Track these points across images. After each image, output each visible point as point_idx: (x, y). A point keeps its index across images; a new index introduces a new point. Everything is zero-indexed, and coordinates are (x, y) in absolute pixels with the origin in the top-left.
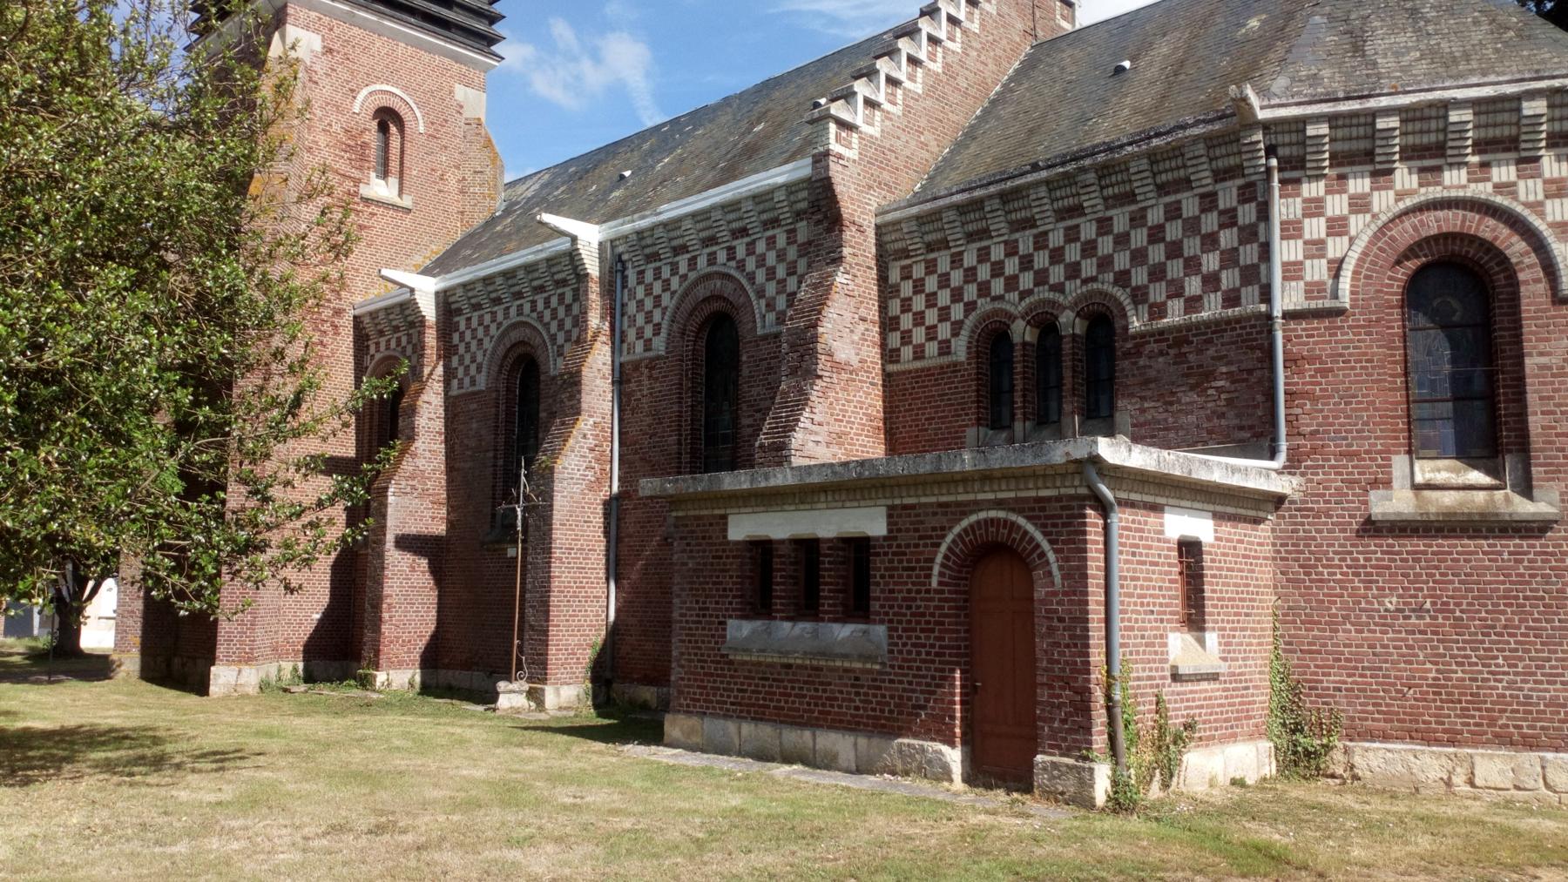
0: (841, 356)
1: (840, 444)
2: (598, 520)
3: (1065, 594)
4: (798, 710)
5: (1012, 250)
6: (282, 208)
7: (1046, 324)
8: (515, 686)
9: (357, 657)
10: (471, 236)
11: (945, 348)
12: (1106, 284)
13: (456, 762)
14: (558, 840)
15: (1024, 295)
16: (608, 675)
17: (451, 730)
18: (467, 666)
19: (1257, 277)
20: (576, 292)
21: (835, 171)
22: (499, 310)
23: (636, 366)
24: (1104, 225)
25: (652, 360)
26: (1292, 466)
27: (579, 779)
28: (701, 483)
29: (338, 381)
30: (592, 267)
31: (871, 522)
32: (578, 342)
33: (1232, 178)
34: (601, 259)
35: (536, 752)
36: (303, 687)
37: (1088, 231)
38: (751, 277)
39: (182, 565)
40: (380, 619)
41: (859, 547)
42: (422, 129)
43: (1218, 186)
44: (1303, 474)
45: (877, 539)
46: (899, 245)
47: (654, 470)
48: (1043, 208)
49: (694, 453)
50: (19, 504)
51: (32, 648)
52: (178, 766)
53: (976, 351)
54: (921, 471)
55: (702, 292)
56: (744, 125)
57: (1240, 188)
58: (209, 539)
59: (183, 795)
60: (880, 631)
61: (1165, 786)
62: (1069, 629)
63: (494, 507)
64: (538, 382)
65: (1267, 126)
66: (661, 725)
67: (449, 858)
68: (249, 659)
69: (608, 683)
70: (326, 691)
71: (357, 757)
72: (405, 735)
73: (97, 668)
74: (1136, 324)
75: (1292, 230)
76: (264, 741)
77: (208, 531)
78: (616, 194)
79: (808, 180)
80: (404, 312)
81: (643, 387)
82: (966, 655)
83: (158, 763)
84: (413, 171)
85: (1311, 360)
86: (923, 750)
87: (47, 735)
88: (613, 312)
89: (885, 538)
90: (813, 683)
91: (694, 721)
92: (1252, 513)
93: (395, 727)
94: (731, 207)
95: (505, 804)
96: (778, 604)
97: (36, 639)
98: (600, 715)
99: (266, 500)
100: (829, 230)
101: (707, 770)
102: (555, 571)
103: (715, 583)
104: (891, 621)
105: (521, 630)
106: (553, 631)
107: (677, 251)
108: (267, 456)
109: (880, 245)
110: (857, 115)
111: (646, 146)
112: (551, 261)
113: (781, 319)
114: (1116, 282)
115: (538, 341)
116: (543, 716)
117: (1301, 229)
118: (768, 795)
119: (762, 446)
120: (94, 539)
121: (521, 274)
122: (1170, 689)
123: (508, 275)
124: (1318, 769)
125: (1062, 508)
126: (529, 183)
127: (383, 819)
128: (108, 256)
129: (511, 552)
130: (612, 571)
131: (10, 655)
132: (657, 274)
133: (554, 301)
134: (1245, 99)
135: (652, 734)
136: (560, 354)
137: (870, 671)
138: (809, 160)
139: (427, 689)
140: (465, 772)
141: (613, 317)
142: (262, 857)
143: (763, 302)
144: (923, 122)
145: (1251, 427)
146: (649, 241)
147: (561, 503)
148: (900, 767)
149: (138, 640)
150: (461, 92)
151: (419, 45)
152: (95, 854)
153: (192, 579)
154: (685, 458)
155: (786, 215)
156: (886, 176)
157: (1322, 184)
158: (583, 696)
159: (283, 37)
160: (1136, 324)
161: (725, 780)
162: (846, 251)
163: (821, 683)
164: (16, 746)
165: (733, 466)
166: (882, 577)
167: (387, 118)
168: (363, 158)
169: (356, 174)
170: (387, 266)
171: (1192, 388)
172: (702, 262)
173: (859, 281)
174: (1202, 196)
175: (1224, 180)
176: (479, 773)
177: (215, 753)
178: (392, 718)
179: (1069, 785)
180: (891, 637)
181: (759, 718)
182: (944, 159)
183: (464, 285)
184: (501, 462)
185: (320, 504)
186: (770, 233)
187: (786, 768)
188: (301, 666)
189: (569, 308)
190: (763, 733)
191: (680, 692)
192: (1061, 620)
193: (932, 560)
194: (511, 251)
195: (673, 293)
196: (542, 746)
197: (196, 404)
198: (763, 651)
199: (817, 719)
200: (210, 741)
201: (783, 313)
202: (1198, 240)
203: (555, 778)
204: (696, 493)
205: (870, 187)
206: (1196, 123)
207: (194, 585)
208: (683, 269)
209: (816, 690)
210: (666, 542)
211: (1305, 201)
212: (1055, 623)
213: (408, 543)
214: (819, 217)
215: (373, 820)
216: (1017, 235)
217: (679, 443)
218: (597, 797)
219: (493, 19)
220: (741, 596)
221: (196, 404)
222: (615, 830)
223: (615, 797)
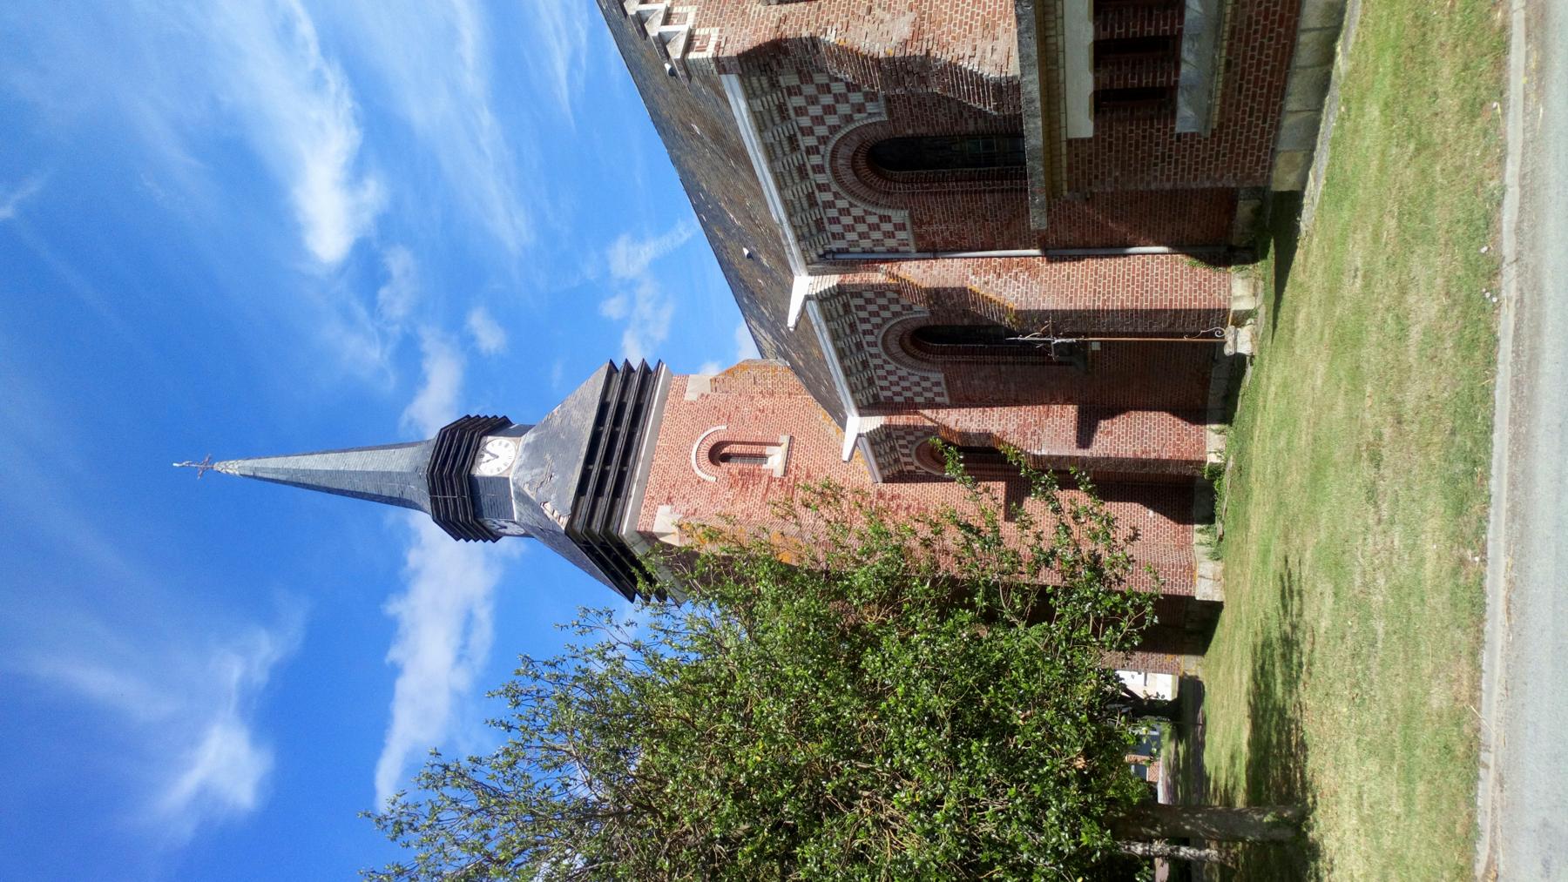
0: (906, 32)
1: (994, 25)
2: (1067, 267)
4: (1276, 50)
6: (804, 537)
8: (1229, 339)
9: (1191, 479)
10: (809, 387)
13: (1307, 390)
14: (1403, 291)
16: (1223, 250)
17: (1271, 396)
18: (1205, 382)
20: (853, 295)
21: (731, 50)
22: (873, 362)
23: (919, 237)
25: (913, 223)
27: (1336, 276)
28: (1036, 167)
29: (950, 497)
30: (831, 281)
32: (899, 292)
34: (824, 273)
35: (1302, 316)
36: (1218, 525)
38: (834, 129)
39: (1112, 620)
40: (1156, 460)
47: (1022, 213)
49: (1001, 177)
50: (1062, 741)
51: (1171, 738)
52: (1294, 627)
55: (849, 177)
56: (695, 143)
58: (1088, 600)
59: (1325, 624)
63: (1052, 363)
64: (936, 327)
66: (1282, 196)
67: (1411, 397)
68: (1190, 569)
69: (1231, 249)
70: (1224, 504)
71: (1295, 478)
72: (1274, 436)
73: (1191, 691)
76: (1272, 557)
77: (1082, 600)
78: (764, 261)
79: (741, 77)
80: (878, 442)
81: (939, 230)
83: (1289, 643)
84: (758, 434)
87: (1255, 728)
90: (1248, 35)
91: (1280, 161)
93: (1272, 443)
94: (770, 153)
95: (1358, 343)
96: (1161, 80)
97: (1162, 734)
98: (1264, 257)
99: (1053, 553)
100: (786, 52)
101: (1335, 143)
102: (1117, 305)
103: (1137, 148)
105: (1172, 335)
106: (1176, 305)
107: (812, 202)
108: (1015, 553)
110: (679, 29)
111: (721, 235)
112: (828, 319)
113: (872, 97)
115: (898, 328)
116: (1262, 311)
118: (1370, 77)
119: (997, 108)
120: (1090, 687)
121: (840, 344)
123: (841, 355)
126: (760, 338)
127: (1365, 455)
128: (854, 668)
129: (1096, 347)
130: (1118, 251)
131: (1177, 753)
132: (835, 221)
133: (863, 314)
135: (1292, 202)
136: (910, 308)
138: (723, 77)
139: (1226, 417)
140: (1319, 382)
141: (875, 261)
142: (1395, 559)
143: (857, 116)
146: (805, 230)
147: (1050, 303)
149: (1169, 657)
150: (691, 396)
151: (656, 430)
152: (1379, 695)
153: (1125, 612)
154: (1007, 185)
155: (774, 99)
158: (1243, 274)
159: (663, 535)
161: (1347, 124)
162: (805, 34)
163: (1249, 26)
164: (1266, 752)
165: (1017, 135)
167: (718, 455)
168: (752, 474)
169: (765, 480)
170: (840, 456)
172: (821, 179)
173: (832, 17)
176: (1321, 368)
177: (1283, 597)
178: (1255, 449)
181: (1282, 92)
183: (853, 393)
184: (1010, 359)
185: (1056, 510)
186: (792, 113)
187: (1339, 59)
188: (1197, 527)
189: (868, 301)
191: (1249, 176)
194: (821, 353)
195: (851, 205)
196: (1296, 310)
197: (972, 606)
198: (1210, 92)
199: (1287, 28)
200: (1269, 598)
201: (866, 94)
203: (1332, 294)
204: (1045, 173)
205: (744, 12)
207: (1131, 611)
208: (828, 197)
209: (1256, 32)
210: (1090, 200)
213: (1084, 439)
214: (774, 63)
215: (1365, 464)
217: (992, 192)
218: (1357, 255)
219: (629, 369)
220: (1152, 119)
221: (972, 606)
222: (1398, 235)
223: (1359, 236)
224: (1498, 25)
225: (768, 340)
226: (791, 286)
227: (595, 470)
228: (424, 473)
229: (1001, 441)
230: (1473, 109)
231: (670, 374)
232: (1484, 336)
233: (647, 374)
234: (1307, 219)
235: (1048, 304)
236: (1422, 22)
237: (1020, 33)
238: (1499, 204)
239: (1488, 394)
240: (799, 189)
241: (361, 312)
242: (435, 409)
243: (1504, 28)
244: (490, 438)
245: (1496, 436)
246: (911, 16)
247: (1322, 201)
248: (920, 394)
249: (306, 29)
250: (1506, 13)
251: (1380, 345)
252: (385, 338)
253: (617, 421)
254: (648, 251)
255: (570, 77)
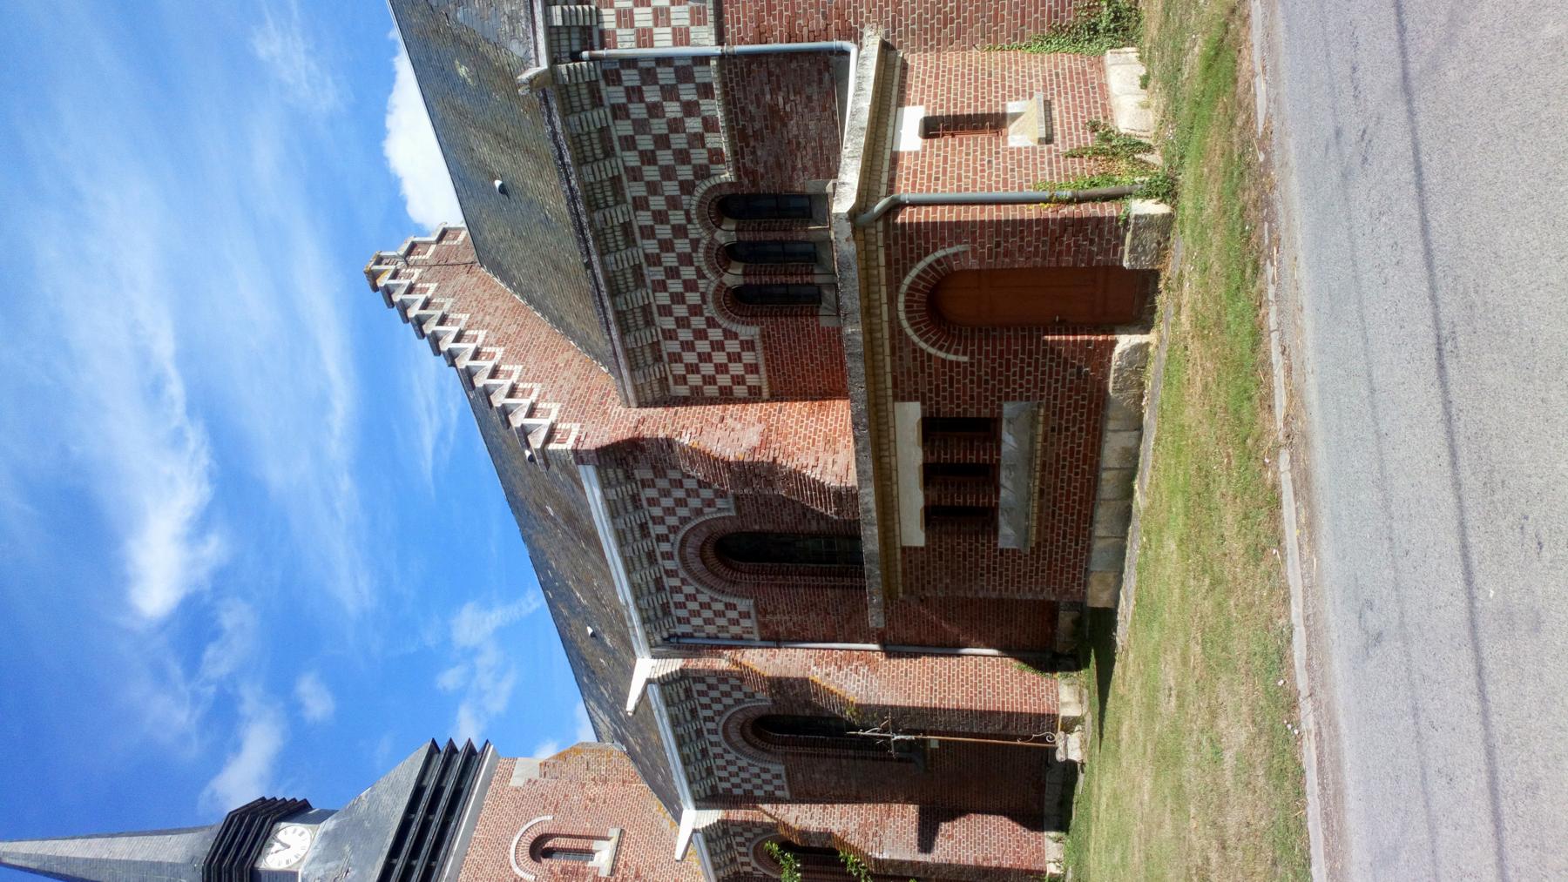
2: (904, 663)
3: (974, 241)
4: (1082, 484)
5: (661, 286)
7: (728, 255)
8: (1060, 744)
11: (748, 345)
12: (692, 202)
13: (1136, 804)
14: (1214, 716)
15: (701, 275)
18: (1040, 787)
19: (684, 69)
21: (590, 444)
22: (712, 751)
23: (763, 626)
24: (640, 204)
25: (758, 612)
26: (854, 35)
27: (1152, 691)
28: (873, 570)
30: (674, 665)
31: (909, 416)
33: (599, 91)
35: (1125, 728)
37: (645, 218)
38: (684, 520)
40: (998, 868)
41: (931, 428)
42: (549, 818)
43: (606, 103)
44: (862, 26)
45: (923, 411)
46: (656, 387)
47: (860, 609)
48: (624, 258)
53: (750, 318)
54: (862, 371)
55: (697, 565)
56: (548, 524)
57: (608, 84)
60: (1008, 408)
61: (1149, 149)
62: (1006, 236)
64: (778, 716)
65: (554, 61)
66: (1097, 612)
69: (1056, 656)
74: (727, 175)
75: (645, 38)
78: (608, 641)
79: (598, 468)
80: (713, 838)
81: (782, 620)
82: (1030, 330)
84: (587, 827)
85: (760, 20)
86: (1120, 369)
88: (715, 646)
89: (923, 403)
92: (897, 71)
95: (1178, 762)
98: (1087, 666)
100: (642, 449)
102: (953, 704)
104: (1000, 398)
106: (1008, 708)
109: (655, 404)
110: (542, 423)
111: (565, 612)
113: (722, 494)
114: (690, 193)
115: (740, 716)
116: (1088, 719)
117: (644, 30)
118: (1165, 514)
119: (837, 513)
121: (680, 730)
122: (1060, 145)
124: (1130, 10)
125: (896, 243)
126: (597, 719)
130: (952, 651)
133: (705, 700)
134: (531, 81)
135: (1107, 618)
136: (753, 695)
137: (1046, 417)
138: (581, 467)
139: (1063, 825)
141: (719, 647)
143: (707, 510)
144: (548, 364)
145: (820, 73)
146: (651, 613)
147: (890, 698)
148: (1134, 391)
150: (517, 781)
154: (847, 582)
155: (629, 488)
156: (594, 398)
157: (604, 11)
158: (1068, 681)
160: (727, 175)
162: (661, 435)
163: (1057, 461)
165: (856, 538)
166: (958, 406)
167: (540, 849)
168: (575, 873)
171: (785, 125)
172: (670, 565)
173: (687, 423)
174: (615, 117)
175: (600, 98)
176: (1148, 784)
178: (1092, 860)
179: (1151, 237)
180: (1014, 399)
181: (1090, 520)
182: (580, 345)
183: (690, 783)
184: (851, 752)
186: (645, 503)
187: (1137, 495)
189: (711, 687)
190: (1104, 517)
192: (998, 245)
193: (944, 361)
194: (659, 738)
196: (1119, 722)
199: (1091, 466)
201: (716, 491)
202: (654, 121)
203: (1151, 712)
204: (882, 576)
205: (605, 412)
206: (551, 122)
208: (676, 582)
211: (619, 26)
212: (1001, 250)
214: (630, 459)
216: (648, 282)
219: (452, 749)
224: (1269, 482)
225: (604, 720)
226: (633, 668)
227: (400, 864)
228: (199, 865)
229: (842, 843)
230: (1257, 553)
231: (496, 757)
232: (1291, 767)
233: (472, 755)
234: (1122, 635)
235: (888, 700)
236: (1204, 473)
237: (857, 452)
238: (1289, 641)
239: (1301, 826)
240: (647, 574)
241: (176, 670)
242: (240, 785)
243: (1275, 486)
244: (283, 824)
245: (1314, 869)
246: (760, 427)
247: (1134, 620)
248: (760, 787)
249: (176, 389)
250: (1275, 473)
251: (1198, 766)
252: (196, 698)
253: (431, 809)
254: (496, 617)
255: (436, 450)
